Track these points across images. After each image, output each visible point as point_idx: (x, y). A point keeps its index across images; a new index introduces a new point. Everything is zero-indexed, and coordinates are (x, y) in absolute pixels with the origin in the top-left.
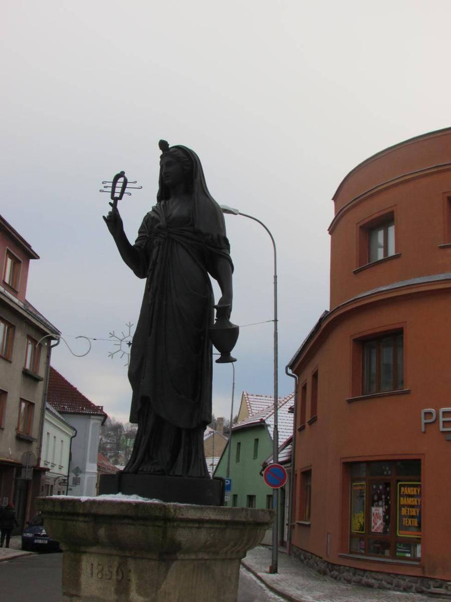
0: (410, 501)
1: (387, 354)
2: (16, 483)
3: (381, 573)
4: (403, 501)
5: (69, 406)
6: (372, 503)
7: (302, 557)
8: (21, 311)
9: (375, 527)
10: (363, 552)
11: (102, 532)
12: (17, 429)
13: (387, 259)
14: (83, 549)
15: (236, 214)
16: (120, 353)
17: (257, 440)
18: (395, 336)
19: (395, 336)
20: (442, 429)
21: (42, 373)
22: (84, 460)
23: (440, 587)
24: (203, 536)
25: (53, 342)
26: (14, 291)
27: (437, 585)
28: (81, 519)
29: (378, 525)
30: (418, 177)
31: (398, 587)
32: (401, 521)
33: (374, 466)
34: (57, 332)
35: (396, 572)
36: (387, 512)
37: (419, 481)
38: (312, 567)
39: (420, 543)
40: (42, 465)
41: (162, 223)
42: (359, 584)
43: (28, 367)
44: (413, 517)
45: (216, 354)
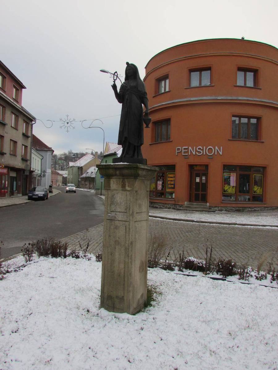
0: (171, 179)
1: (164, 127)
2: (23, 176)
4: (169, 179)
5: (39, 148)
6: (158, 180)
8: (20, 110)
9: (159, 188)
10: (154, 196)
11: (118, 172)
12: (22, 156)
13: (165, 92)
14: (111, 177)
15: (108, 73)
18: (167, 121)
19: (167, 121)
20: (183, 154)
21: (29, 134)
22: (46, 168)
23: (181, 207)
24: (144, 173)
25: (33, 122)
26: (17, 102)
27: (179, 206)
28: (111, 169)
29: (160, 187)
30: (178, 61)
31: (166, 208)
34: (35, 119)
35: (165, 203)
36: (163, 183)
37: (175, 172)
40: (32, 170)
41: (129, 87)
44: (172, 184)
45: (145, 125)
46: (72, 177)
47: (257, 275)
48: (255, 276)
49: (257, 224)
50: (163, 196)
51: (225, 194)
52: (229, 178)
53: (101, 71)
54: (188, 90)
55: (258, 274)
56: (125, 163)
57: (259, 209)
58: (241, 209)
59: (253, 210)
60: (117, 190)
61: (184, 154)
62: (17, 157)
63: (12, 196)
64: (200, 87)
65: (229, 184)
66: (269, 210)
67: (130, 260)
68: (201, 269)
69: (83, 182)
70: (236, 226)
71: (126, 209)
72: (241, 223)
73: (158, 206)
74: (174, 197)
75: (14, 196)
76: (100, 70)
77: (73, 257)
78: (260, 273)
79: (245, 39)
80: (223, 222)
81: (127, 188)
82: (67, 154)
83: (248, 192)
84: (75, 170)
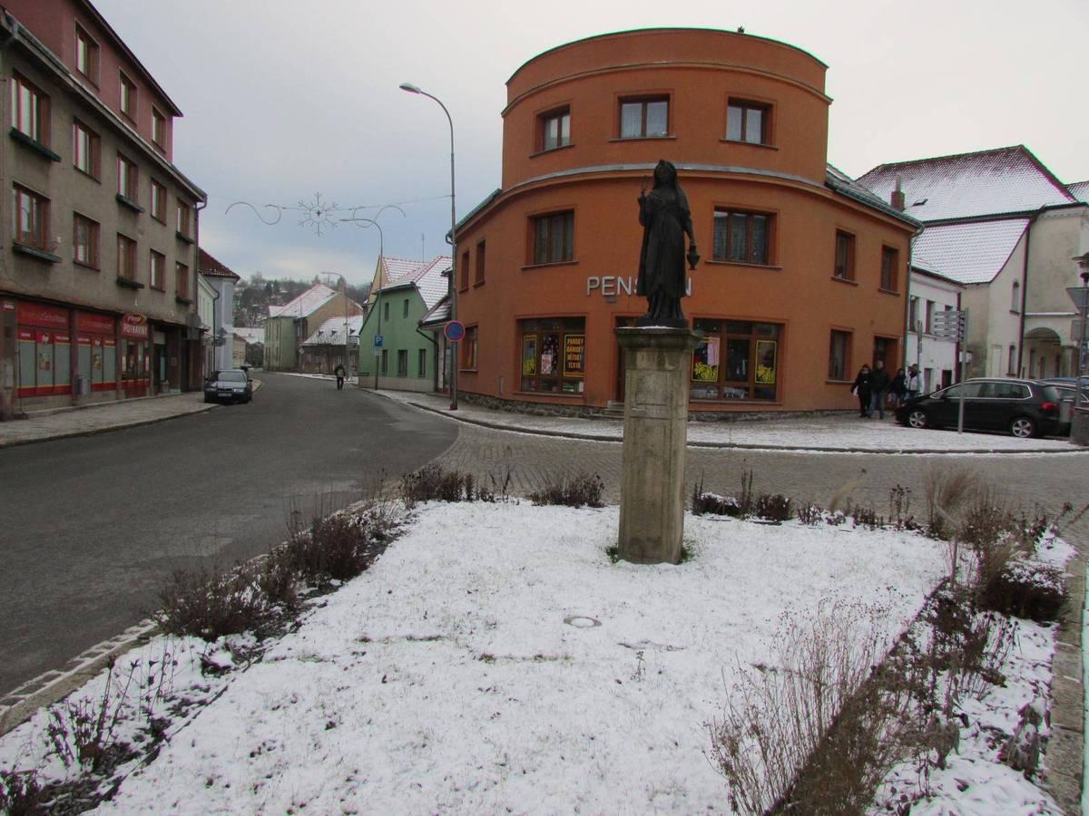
0: (574, 349)
4: (569, 349)
6: (542, 351)
7: (467, 398)
11: (653, 341)
17: (407, 301)
18: (567, 215)
19: (567, 215)
23: (598, 413)
25: (199, 205)
26: (164, 152)
29: (547, 368)
31: (564, 414)
32: (567, 364)
33: (542, 322)
36: (555, 358)
37: (584, 333)
38: (481, 405)
39: (582, 381)
42: (531, 413)
43: (179, 230)
46: (277, 344)
47: (831, 518)
48: (827, 518)
49: (775, 444)
50: (554, 389)
52: (706, 347)
54: (617, 145)
55: (832, 515)
56: (664, 327)
57: (768, 415)
58: (730, 415)
59: (755, 418)
60: (648, 370)
61: (607, 294)
63: (160, 395)
64: (643, 139)
66: (789, 418)
67: (672, 480)
68: (732, 511)
71: (665, 400)
72: (744, 443)
74: (581, 389)
75: (164, 395)
76: (402, 83)
77: (485, 500)
78: (835, 514)
80: (705, 441)
81: (667, 366)
82: (249, 283)
84: (286, 325)
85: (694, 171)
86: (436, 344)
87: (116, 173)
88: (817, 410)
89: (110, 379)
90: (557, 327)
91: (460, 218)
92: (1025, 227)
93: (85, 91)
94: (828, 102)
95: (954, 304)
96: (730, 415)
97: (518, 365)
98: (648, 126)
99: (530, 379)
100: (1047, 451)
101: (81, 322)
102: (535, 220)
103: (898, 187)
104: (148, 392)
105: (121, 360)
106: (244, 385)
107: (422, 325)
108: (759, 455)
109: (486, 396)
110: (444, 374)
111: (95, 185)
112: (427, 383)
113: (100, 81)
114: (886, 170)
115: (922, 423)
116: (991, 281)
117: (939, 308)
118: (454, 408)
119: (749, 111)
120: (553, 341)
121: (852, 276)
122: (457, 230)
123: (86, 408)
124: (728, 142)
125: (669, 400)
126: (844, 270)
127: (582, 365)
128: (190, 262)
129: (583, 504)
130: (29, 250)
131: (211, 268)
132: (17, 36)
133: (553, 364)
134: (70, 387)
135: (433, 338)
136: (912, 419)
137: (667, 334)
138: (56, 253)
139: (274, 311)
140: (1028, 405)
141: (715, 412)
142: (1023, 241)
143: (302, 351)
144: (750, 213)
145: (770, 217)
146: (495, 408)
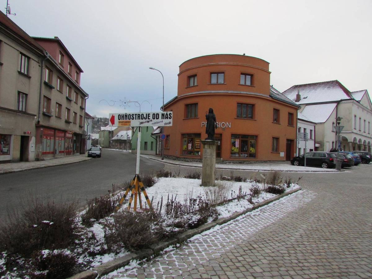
0: (198, 143)
3: (191, 158)
6: (188, 143)
7: (166, 157)
11: (208, 143)
16: (126, 106)
18: (196, 104)
19: (196, 104)
25: (86, 98)
29: (190, 148)
31: (195, 161)
32: (196, 147)
33: (189, 135)
34: (88, 95)
36: (192, 145)
38: (170, 159)
46: (103, 139)
50: (192, 154)
51: (233, 153)
52: (235, 142)
53: (150, 68)
54: (210, 86)
57: (253, 162)
58: (242, 162)
62: (77, 125)
63: (74, 155)
65: (235, 146)
66: (260, 163)
68: (228, 180)
69: (114, 143)
70: (240, 170)
73: (189, 160)
74: (200, 154)
79: (245, 55)
83: (246, 151)
84: (107, 133)
85: (231, 93)
86: (156, 140)
87: (66, 89)
88: (268, 161)
89: (63, 150)
90: (193, 136)
91: (165, 103)
92: (336, 106)
93: (61, 68)
94: (270, 73)
95: (313, 129)
96: (242, 162)
97: (182, 146)
98: (219, 80)
99: (185, 151)
100: (326, 171)
101: (57, 134)
102: (187, 106)
103: (298, 93)
104: (71, 154)
105: (65, 144)
106: (100, 152)
107: (152, 134)
108: (246, 171)
109: (172, 156)
110: (159, 149)
111: (61, 94)
112: (154, 152)
113: (64, 66)
114: (296, 87)
115: (297, 164)
116: (325, 122)
117: (308, 132)
118: (163, 159)
119: (247, 76)
120: (192, 140)
121: (279, 122)
122: (165, 106)
123: (57, 158)
124: (241, 85)
125: (211, 155)
126: (276, 120)
127: (200, 147)
128: (83, 115)
129: (196, 178)
130: (46, 114)
131: (88, 116)
132: (48, 57)
133: (192, 147)
134: (53, 152)
135: (155, 138)
136: (295, 163)
137: (210, 142)
138: (52, 114)
139: (103, 128)
140: (327, 159)
141: (238, 161)
142: (336, 109)
143: (111, 142)
144: (247, 104)
145: (253, 106)
146: (175, 160)
